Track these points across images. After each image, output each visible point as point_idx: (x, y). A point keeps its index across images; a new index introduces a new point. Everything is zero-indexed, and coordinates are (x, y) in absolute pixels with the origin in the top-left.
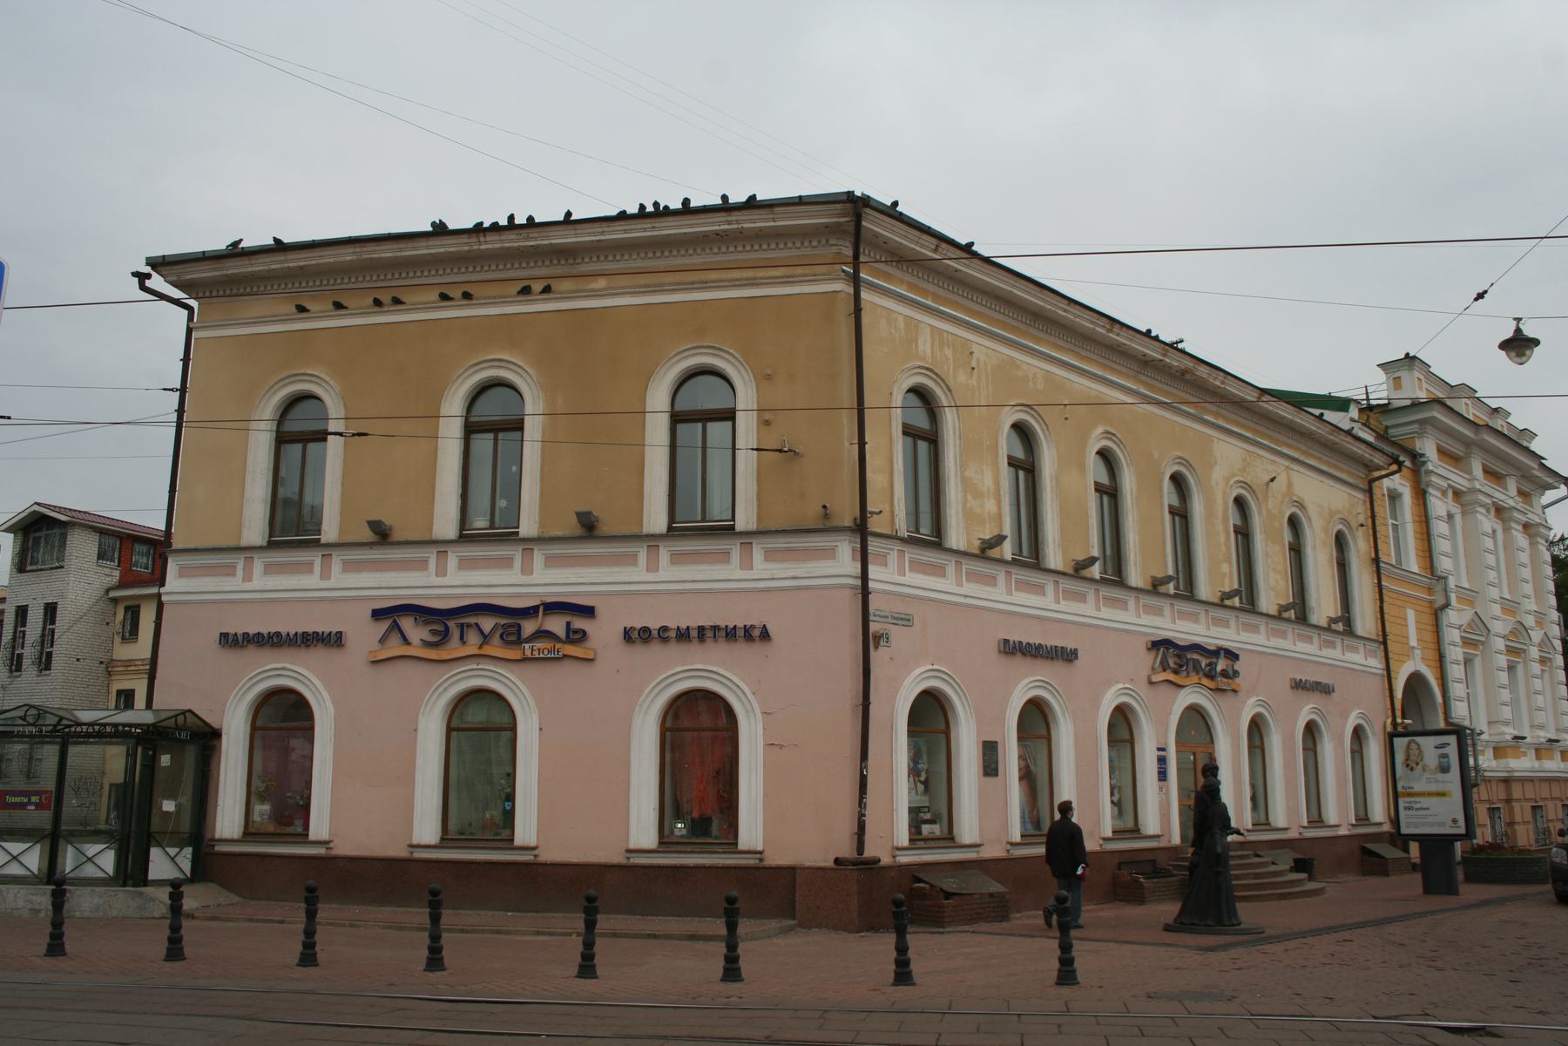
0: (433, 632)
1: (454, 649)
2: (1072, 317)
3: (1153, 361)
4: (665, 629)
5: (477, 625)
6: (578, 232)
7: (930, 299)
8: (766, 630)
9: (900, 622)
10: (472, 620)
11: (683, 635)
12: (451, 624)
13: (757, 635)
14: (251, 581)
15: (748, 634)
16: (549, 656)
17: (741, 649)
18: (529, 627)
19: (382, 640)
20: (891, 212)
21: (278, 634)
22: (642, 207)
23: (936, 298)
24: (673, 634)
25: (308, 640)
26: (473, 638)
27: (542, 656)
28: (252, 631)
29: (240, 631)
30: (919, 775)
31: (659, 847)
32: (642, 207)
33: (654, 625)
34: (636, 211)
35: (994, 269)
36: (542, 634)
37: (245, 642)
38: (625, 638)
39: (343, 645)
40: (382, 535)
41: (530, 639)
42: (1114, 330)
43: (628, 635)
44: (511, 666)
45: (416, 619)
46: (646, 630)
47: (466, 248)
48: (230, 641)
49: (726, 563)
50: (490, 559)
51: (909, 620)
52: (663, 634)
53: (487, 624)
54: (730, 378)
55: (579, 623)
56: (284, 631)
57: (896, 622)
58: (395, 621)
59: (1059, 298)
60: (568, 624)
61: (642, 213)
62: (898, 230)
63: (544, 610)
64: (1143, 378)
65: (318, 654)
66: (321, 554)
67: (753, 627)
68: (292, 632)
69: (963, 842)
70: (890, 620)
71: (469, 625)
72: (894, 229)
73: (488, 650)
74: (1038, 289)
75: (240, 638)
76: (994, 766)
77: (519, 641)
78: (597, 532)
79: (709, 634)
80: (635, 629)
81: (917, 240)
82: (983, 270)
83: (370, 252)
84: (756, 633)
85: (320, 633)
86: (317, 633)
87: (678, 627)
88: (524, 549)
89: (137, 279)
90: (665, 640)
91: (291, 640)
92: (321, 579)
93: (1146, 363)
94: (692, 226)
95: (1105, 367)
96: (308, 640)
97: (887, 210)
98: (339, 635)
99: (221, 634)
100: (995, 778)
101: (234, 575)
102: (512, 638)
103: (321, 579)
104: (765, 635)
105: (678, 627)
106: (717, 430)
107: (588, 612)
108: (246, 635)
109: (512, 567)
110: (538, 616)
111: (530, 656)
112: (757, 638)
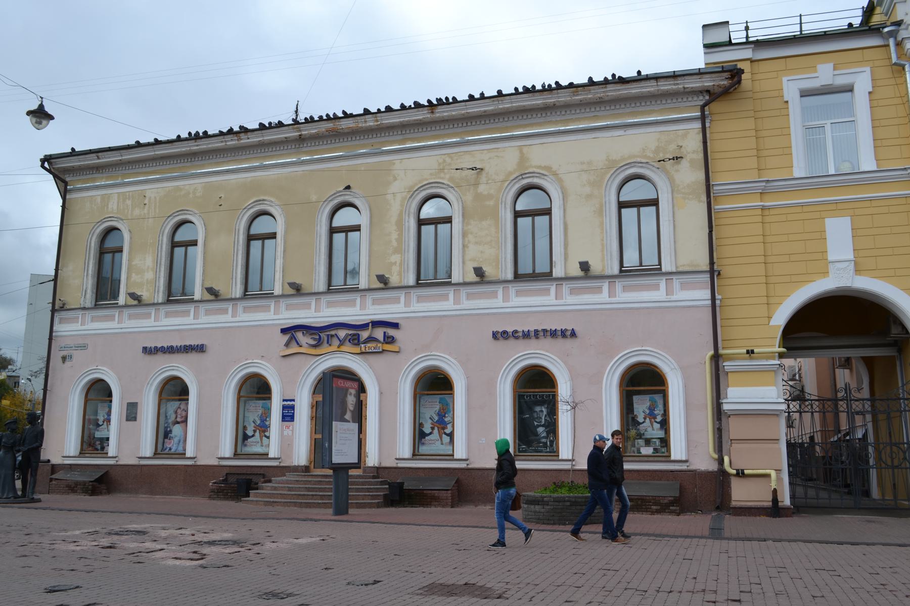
0: (315, 339)
1: (325, 349)
4: (516, 332)
5: (336, 334)
8: (574, 332)
9: (79, 348)
10: (333, 333)
11: (526, 335)
12: (322, 335)
13: (200, 349)
15: (563, 334)
16: (374, 351)
17: (560, 342)
18: (365, 335)
19: (287, 345)
20: (640, 77)
21: (172, 347)
24: (520, 334)
25: (188, 349)
26: (336, 342)
27: (370, 351)
28: (159, 346)
29: (153, 346)
30: (655, 418)
32: (516, 89)
33: (510, 330)
36: (371, 339)
37: (155, 352)
38: (493, 337)
39: (204, 351)
40: (297, 290)
41: (366, 341)
43: (495, 335)
44: (359, 355)
45: (303, 333)
46: (505, 332)
48: (148, 351)
49: (308, 309)
50: (388, 298)
51: (85, 347)
52: (515, 335)
53: (342, 333)
54: (446, 197)
55: (391, 332)
56: (175, 345)
57: (77, 348)
58: (292, 334)
60: (385, 333)
63: (372, 325)
64: (304, 149)
66: (194, 306)
67: (566, 330)
70: (74, 348)
71: (332, 336)
73: (343, 348)
75: (153, 350)
76: (133, 415)
78: (486, 279)
79: (541, 334)
80: (498, 332)
82: (130, 153)
84: (568, 333)
85: (193, 345)
86: (191, 345)
87: (523, 330)
88: (556, 285)
89: (70, 151)
90: (517, 338)
91: (178, 349)
92: (232, 317)
96: (188, 349)
97: (612, 81)
99: (143, 347)
100: (135, 422)
101: (399, 303)
102: (356, 341)
103: (232, 317)
104: (573, 334)
105: (523, 330)
107: (395, 326)
108: (156, 347)
109: (549, 295)
110: (368, 329)
111: (364, 351)
112: (569, 336)
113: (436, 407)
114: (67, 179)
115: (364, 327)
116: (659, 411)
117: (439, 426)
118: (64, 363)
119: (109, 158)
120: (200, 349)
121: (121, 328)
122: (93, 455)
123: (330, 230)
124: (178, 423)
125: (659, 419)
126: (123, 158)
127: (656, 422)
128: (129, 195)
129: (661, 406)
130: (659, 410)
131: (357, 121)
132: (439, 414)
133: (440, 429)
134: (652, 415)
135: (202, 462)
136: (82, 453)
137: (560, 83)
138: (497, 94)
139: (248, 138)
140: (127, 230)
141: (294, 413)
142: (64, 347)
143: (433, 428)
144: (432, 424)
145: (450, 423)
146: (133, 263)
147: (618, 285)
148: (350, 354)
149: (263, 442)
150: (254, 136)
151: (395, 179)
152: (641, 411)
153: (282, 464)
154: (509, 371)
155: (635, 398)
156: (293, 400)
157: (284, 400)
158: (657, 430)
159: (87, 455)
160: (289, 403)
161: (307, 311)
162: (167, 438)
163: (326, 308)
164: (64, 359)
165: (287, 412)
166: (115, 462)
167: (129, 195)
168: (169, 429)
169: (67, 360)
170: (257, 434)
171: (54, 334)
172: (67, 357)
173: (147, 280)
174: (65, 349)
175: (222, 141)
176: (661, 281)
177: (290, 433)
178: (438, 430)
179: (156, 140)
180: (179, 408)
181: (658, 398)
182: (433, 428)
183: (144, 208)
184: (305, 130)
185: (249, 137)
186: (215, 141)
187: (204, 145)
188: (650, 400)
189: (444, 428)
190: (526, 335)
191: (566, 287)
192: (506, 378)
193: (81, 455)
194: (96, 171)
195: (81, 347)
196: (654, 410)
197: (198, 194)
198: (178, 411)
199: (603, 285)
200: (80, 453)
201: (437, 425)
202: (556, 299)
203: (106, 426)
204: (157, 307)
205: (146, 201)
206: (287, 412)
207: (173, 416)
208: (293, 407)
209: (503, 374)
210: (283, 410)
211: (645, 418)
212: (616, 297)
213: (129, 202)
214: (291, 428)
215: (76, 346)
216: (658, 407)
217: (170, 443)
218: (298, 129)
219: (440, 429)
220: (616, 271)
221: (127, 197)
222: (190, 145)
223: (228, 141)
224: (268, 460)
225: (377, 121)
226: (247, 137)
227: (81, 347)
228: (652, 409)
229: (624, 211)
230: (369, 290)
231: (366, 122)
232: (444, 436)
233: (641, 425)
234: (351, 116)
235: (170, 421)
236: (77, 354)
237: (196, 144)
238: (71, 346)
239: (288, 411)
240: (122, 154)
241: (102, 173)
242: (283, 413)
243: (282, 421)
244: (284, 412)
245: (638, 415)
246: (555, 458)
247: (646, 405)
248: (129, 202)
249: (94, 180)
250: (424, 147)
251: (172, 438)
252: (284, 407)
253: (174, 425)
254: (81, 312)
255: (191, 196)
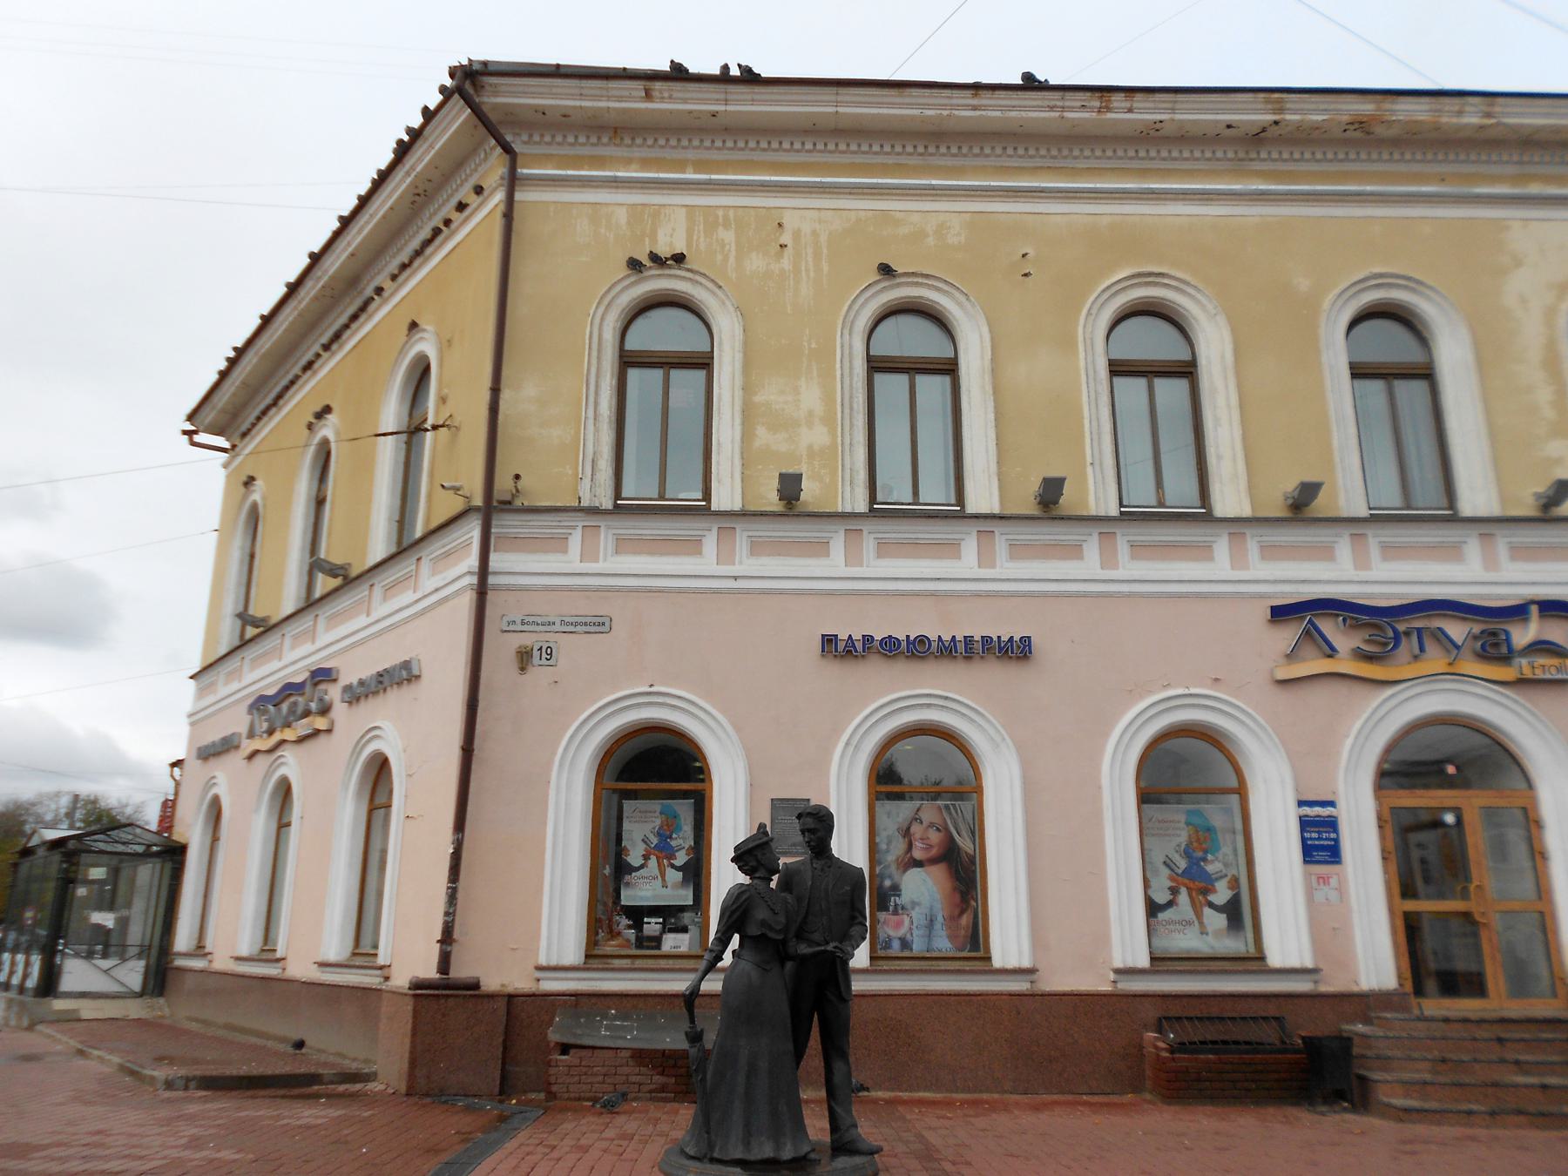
2: (998, 114)
3: (1264, 130)
6: (839, 98)
7: (690, 169)
9: (579, 628)
10: (1437, 623)
13: (1017, 651)
14: (1117, 569)
19: (1292, 656)
22: (726, 68)
23: (700, 166)
30: (671, 856)
31: (1152, 965)
32: (726, 68)
34: (717, 72)
35: (775, 89)
42: (1115, 104)
47: (296, 313)
59: (947, 92)
61: (724, 77)
62: (559, 90)
64: (1257, 166)
65: (992, 674)
68: (947, 637)
69: (1043, 988)
72: (554, 90)
74: (893, 92)
75: (859, 646)
77: (1506, 659)
78: (800, 508)
81: (604, 93)
83: (262, 346)
85: (843, 636)
93: (1258, 138)
94: (389, 196)
95: (1144, 173)
98: (1026, 642)
106: (686, 383)
113: (1179, 836)
114: (517, 147)
115: (1518, 612)
116: (683, 839)
117: (1191, 885)
118: (523, 669)
119: (685, 101)
120: (1017, 651)
121: (736, 578)
122: (639, 963)
123: (621, 357)
124: (919, 864)
125: (681, 858)
126: (730, 108)
127: (673, 866)
128: (726, 217)
129: (687, 829)
130: (684, 839)
131: (1439, 107)
132: (1187, 854)
133: (1194, 894)
134: (663, 850)
135: (1063, 979)
136: (593, 957)
137: (756, 70)
138: (1021, 82)
139: (1130, 110)
140: (732, 309)
141: (1336, 841)
142: (523, 623)
143: (1174, 891)
144: (1171, 879)
145: (1221, 877)
146: (758, 399)
147: (606, 537)
148: (1482, 682)
149: (1205, 921)
150: (1152, 105)
151: (1518, 263)
152: (638, 837)
153: (1323, 988)
154: (1131, 739)
155: (628, 805)
156: (1332, 804)
157: (1301, 803)
158: (675, 886)
159: (617, 963)
160: (1318, 810)
161: (560, 557)
162: (886, 909)
163: (612, 556)
164: (524, 658)
165: (1315, 835)
166: (280, 971)
167: (726, 217)
168: (887, 883)
169: (536, 660)
170: (1183, 898)
171: (491, 580)
172: (536, 653)
173: (810, 447)
174: (525, 628)
175: (1055, 106)
176: (706, 533)
177: (1333, 895)
178: (1190, 896)
179: (1028, 78)
180: (916, 819)
181: (684, 809)
182: (1174, 891)
183: (779, 256)
184: (1295, 112)
185: (1135, 105)
186: (1035, 103)
187: (744, 104)
188: (661, 813)
189: (1206, 891)
190: (946, 648)
191: (742, 535)
192: (1125, 753)
193: (595, 963)
194: (610, 139)
195: (586, 624)
196: (671, 837)
197: (952, 240)
198: (913, 829)
199: (1334, 542)
200: (587, 956)
201: (1186, 881)
202: (979, 567)
203: (656, 872)
204: (592, 521)
205: (786, 238)
206: (1315, 835)
207: (899, 847)
208: (1331, 824)
209: (572, 737)
210: (1303, 830)
211: (646, 857)
212: (734, 564)
213: (728, 236)
214: (1334, 881)
215: (567, 619)
216: (681, 829)
217: (899, 925)
218: (1277, 106)
219: (1194, 894)
220: (862, 506)
221: (721, 220)
222: (955, 101)
223: (1072, 109)
224: (996, 977)
225: (1488, 115)
226: (1128, 105)
227: (586, 624)
228: (665, 835)
229: (633, 375)
230: (743, 514)
231: (1460, 113)
232: (1207, 911)
233: (634, 874)
234: (1045, 87)
235: (891, 858)
236: (570, 649)
237: (975, 102)
238: (546, 620)
239: (1318, 832)
240: (729, 97)
241: (981, 154)
242: (1304, 840)
243: (1305, 862)
244: (1307, 835)
245: (629, 847)
246: (978, 965)
247: (652, 825)
248: (728, 236)
249: (599, 162)
250: (562, 180)
251: (903, 908)
252: (1305, 824)
253: (905, 871)
254: (580, 522)
255: (931, 241)
